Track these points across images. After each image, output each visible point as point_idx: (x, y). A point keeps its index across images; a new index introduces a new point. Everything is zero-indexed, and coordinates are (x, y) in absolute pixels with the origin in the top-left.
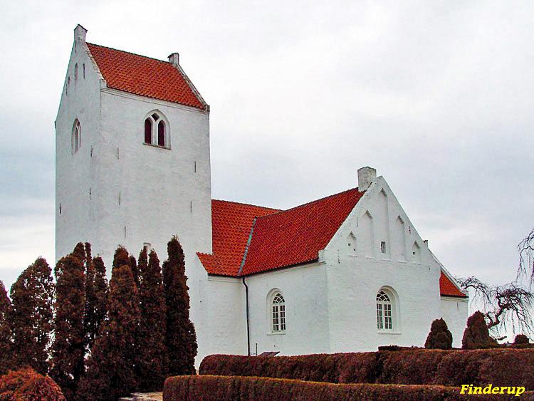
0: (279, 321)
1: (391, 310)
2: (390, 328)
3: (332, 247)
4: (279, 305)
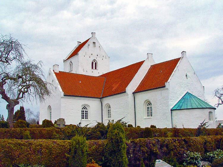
0: (150, 113)
1: (88, 115)
2: (87, 119)
3: (103, 46)
4: (150, 106)
